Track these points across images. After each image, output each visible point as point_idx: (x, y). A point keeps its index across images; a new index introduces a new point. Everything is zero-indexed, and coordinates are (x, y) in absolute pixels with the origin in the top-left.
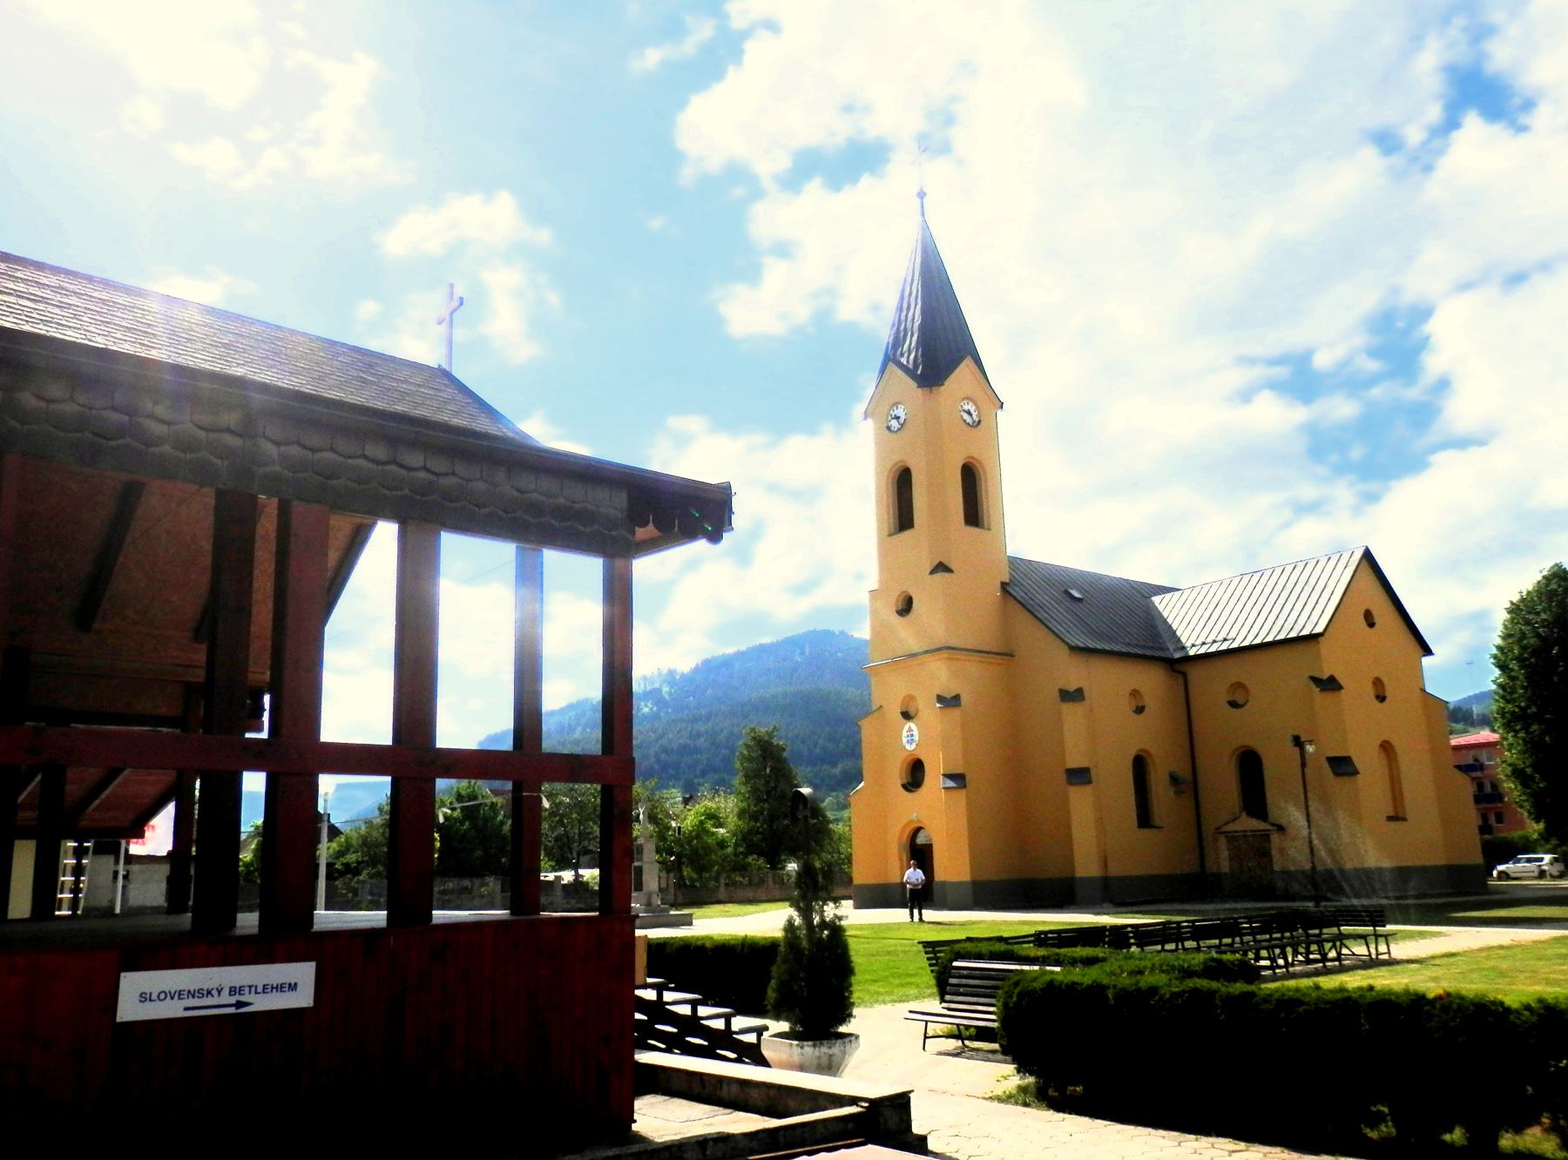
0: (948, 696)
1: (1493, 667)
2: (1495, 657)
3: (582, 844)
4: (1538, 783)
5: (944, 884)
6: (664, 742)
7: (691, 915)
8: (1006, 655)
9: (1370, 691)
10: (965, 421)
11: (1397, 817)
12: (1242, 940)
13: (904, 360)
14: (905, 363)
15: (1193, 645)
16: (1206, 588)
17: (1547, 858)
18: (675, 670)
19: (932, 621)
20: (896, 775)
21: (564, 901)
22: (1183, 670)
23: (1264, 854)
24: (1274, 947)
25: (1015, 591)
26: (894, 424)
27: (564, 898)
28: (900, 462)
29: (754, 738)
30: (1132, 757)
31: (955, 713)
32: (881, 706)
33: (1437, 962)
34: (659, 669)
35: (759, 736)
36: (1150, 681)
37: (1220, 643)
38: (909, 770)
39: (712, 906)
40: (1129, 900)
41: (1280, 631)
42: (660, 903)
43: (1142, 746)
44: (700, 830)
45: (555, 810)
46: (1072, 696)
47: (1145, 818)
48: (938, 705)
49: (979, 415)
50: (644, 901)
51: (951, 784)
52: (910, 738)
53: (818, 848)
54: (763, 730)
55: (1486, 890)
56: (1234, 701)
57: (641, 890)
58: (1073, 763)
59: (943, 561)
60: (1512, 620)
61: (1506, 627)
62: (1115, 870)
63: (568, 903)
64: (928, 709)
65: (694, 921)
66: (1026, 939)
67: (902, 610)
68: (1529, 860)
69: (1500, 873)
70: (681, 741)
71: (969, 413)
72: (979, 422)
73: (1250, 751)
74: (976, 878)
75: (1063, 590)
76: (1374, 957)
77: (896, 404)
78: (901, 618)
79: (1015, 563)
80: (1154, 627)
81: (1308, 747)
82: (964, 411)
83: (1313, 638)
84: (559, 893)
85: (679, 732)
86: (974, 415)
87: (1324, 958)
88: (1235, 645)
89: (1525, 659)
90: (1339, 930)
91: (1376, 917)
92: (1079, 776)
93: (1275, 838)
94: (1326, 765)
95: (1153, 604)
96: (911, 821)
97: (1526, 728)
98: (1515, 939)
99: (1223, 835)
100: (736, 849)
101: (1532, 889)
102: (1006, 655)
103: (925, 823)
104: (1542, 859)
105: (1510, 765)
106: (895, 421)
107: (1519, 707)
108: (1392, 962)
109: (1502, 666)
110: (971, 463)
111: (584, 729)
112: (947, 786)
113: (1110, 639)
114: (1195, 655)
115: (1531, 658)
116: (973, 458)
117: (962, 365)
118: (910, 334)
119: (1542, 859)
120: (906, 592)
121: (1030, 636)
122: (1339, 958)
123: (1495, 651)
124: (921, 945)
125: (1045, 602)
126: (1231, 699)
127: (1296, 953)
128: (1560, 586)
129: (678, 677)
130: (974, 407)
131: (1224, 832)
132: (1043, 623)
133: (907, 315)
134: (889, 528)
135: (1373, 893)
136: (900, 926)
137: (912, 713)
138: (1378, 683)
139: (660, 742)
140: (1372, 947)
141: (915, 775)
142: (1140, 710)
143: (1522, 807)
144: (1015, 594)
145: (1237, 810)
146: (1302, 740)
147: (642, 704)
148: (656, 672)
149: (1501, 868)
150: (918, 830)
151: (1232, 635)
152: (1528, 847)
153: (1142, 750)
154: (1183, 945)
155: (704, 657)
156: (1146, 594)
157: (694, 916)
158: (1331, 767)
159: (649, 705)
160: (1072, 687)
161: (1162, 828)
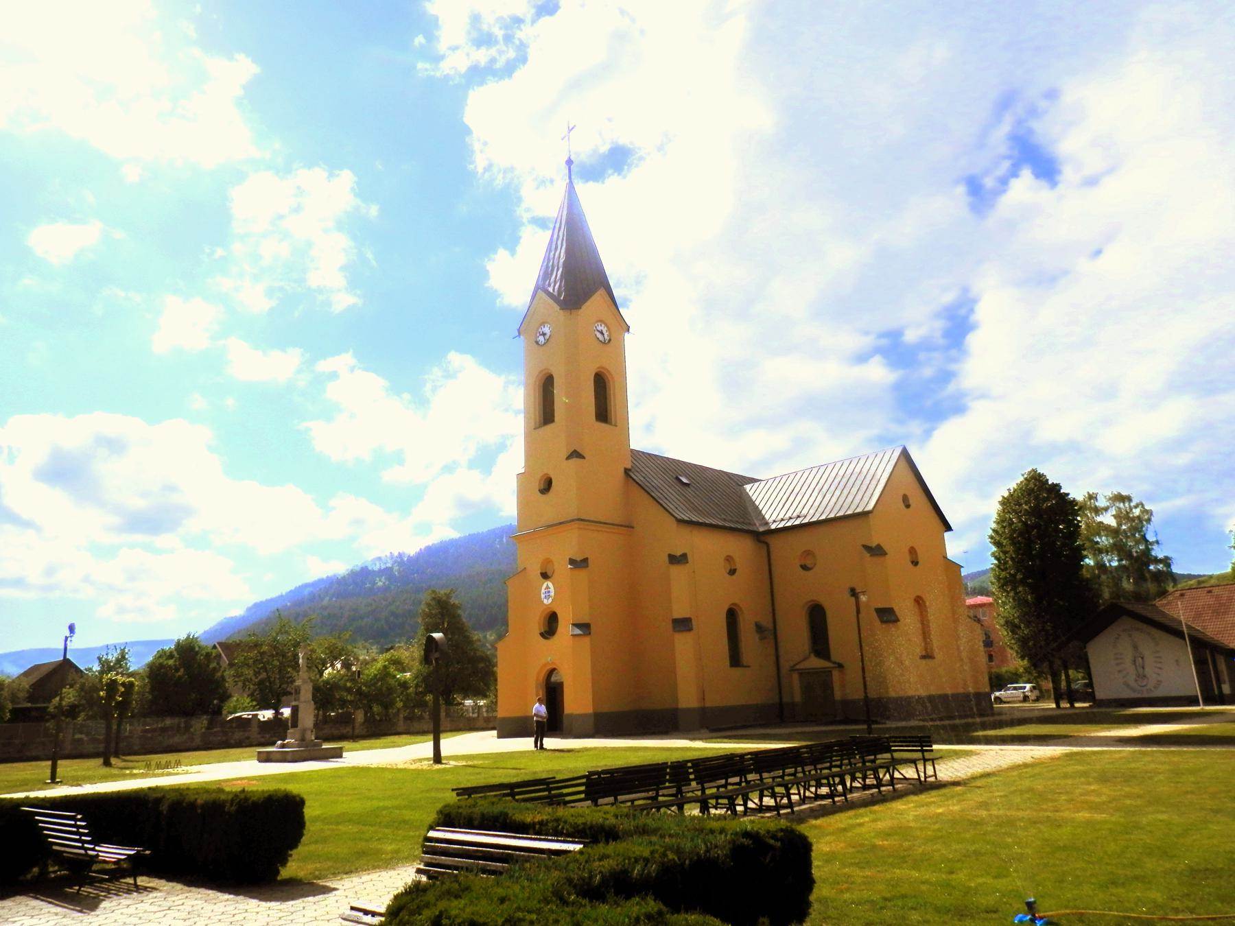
0: (578, 559)
1: (990, 545)
2: (991, 537)
4: (1023, 630)
5: (570, 716)
7: (341, 749)
8: (628, 527)
9: (908, 558)
10: (598, 338)
11: (927, 656)
12: (803, 769)
13: (551, 289)
14: (552, 291)
15: (774, 521)
16: (784, 479)
17: (1028, 686)
18: (404, 553)
19: (565, 501)
20: (536, 625)
21: (259, 736)
22: (766, 541)
23: (827, 686)
24: (833, 776)
26: (541, 339)
27: (259, 733)
28: (545, 369)
29: (434, 599)
30: (725, 611)
31: (582, 574)
32: (525, 568)
33: (979, 783)
34: (391, 553)
36: (740, 548)
39: (389, 737)
40: (724, 726)
42: (313, 738)
43: (736, 601)
44: (385, 674)
45: (259, 658)
46: (678, 560)
47: (735, 659)
48: (569, 566)
49: (610, 335)
50: (298, 736)
51: (578, 631)
53: (485, 688)
54: (442, 592)
55: (992, 712)
58: (679, 613)
60: (1004, 509)
61: (999, 515)
62: (711, 702)
63: (263, 737)
64: (562, 568)
66: (569, 783)
67: (544, 489)
68: (1015, 689)
69: (996, 698)
70: (406, 607)
71: (602, 333)
73: (818, 605)
74: (600, 710)
76: (923, 779)
77: (543, 324)
80: (745, 508)
81: (862, 597)
82: (598, 331)
83: (865, 514)
84: (255, 729)
85: (404, 600)
87: (880, 784)
88: (806, 521)
89: (1015, 538)
90: (892, 755)
91: (922, 741)
92: (683, 624)
95: (745, 490)
97: (1014, 589)
98: (1035, 756)
99: (796, 672)
100: (416, 689)
101: (1021, 710)
102: (628, 527)
104: (1025, 688)
105: (1003, 617)
107: (1010, 573)
108: (939, 786)
109: (997, 544)
110: (603, 372)
111: (331, 599)
112: (575, 633)
114: (776, 529)
115: (1018, 537)
116: (603, 368)
117: (598, 293)
118: (556, 268)
119: (1025, 688)
120: (547, 474)
121: (647, 512)
123: (990, 532)
125: (659, 485)
127: (853, 779)
128: (1036, 486)
130: (606, 329)
131: (798, 670)
133: (554, 255)
134: (535, 423)
137: (549, 574)
138: (912, 551)
140: (921, 767)
141: (551, 624)
142: (732, 572)
143: (1012, 648)
144: (635, 477)
146: (858, 591)
148: (388, 555)
149: (997, 694)
150: (552, 671)
151: (805, 512)
152: (1015, 678)
154: (746, 778)
155: (427, 545)
156: (740, 484)
158: (879, 616)
159: (383, 579)
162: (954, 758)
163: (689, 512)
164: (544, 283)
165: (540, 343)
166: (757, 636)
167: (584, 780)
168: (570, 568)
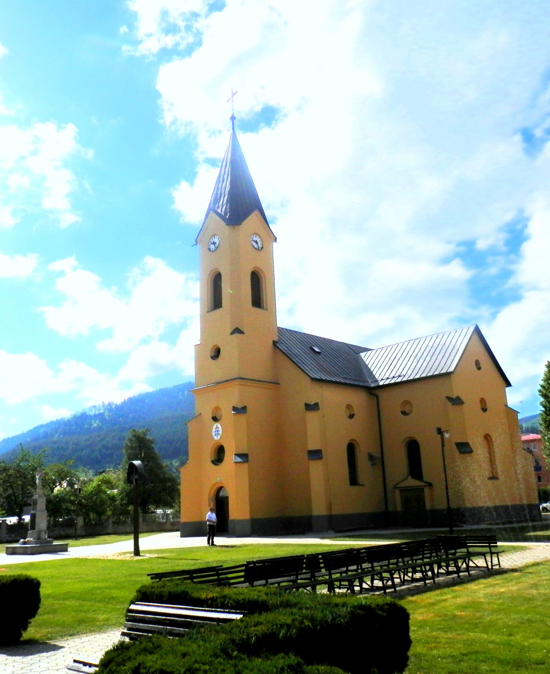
0: (240, 407)
1: (539, 397)
2: (540, 391)
3: (24, 499)
5: (233, 521)
6: (104, 442)
9: (479, 406)
10: (254, 246)
11: (494, 477)
12: (403, 560)
13: (219, 211)
14: (220, 212)
15: (382, 379)
18: (112, 403)
20: (208, 455)
21: (7, 536)
22: (376, 394)
23: (420, 499)
25: (282, 347)
26: (212, 247)
27: (7, 534)
31: (242, 418)
32: (201, 414)
34: (103, 402)
35: (138, 434)
37: (397, 378)
38: (216, 453)
40: (345, 529)
41: (430, 371)
42: (46, 537)
44: (98, 491)
45: (7, 479)
46: (312, 407)
47: (354, 480)
48: (233, 412)
49: (262, 244)
50: (35, 536)
51: (239, 460)
52: (217, 433)
54: (140, 431)
56: (404, 411)
57: (34, 529)
59: (238, 327)
61: (546, 375)
63: (9, 537)
64: (227, 414)
65: (69, 549)
66: (233, 570)
71: (256, 242)
72: (262, 248)
75: (309, 347)
76: (490, 567)
77: (214, 236)
78: (214, 361)
79: (281, 331)
80: (361, 370)
82: (254, 241)
85: (113, 437)
86: (259, 243)
87: (459, 570)
88: (405, 379)
90: (468, 550)
92: (316, 454)
93: (427, 491)
94: (455, 447)
96: (217, 483)
99: (398, 489)
103: (225, 485)
106: (213, 245)
108: (502, 572)
111: (59, 436)
112: (237, 461)
113: (335, 375)
116: (257, 268)
120: (217, 345)
122: (468, 569)
124: (149, 578)
126: (403, 410)
127: (440, 567)
129: (114, 407)
130: (259, 239)
132: (290, 359)
133: (222, 185)
134: (208, 308)
135: (480, 521)
136: (199, 549)
137: (218, 418)
138: (483, 401)
139: (102, 443)
140: (489, 558)
142: (351, 416)
145: (406, 475)
146: (442, 430)
147: (93, 421)
150: (220, 489)
151: (404, 373)
153: (351, 440)
154: (361, 566)
156: (357, 352)
157: (69, 545)
158: (458, 448)
159: (97, 421)
160: (312, 403)
161: (363, 485)
162: (513, 551)
163: (320, 373)
164: (214, 206)
165: (211, 250)
166: (369, 463)
167: (244, 568)
168: (234, 414)
